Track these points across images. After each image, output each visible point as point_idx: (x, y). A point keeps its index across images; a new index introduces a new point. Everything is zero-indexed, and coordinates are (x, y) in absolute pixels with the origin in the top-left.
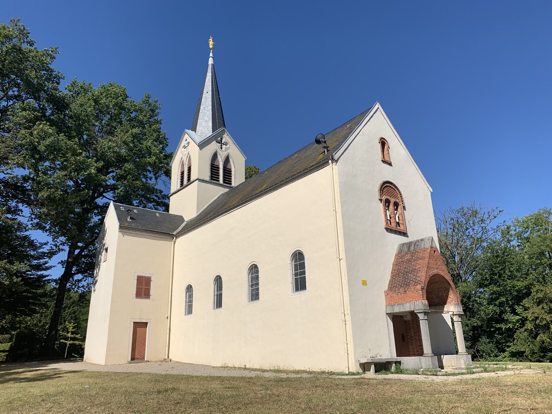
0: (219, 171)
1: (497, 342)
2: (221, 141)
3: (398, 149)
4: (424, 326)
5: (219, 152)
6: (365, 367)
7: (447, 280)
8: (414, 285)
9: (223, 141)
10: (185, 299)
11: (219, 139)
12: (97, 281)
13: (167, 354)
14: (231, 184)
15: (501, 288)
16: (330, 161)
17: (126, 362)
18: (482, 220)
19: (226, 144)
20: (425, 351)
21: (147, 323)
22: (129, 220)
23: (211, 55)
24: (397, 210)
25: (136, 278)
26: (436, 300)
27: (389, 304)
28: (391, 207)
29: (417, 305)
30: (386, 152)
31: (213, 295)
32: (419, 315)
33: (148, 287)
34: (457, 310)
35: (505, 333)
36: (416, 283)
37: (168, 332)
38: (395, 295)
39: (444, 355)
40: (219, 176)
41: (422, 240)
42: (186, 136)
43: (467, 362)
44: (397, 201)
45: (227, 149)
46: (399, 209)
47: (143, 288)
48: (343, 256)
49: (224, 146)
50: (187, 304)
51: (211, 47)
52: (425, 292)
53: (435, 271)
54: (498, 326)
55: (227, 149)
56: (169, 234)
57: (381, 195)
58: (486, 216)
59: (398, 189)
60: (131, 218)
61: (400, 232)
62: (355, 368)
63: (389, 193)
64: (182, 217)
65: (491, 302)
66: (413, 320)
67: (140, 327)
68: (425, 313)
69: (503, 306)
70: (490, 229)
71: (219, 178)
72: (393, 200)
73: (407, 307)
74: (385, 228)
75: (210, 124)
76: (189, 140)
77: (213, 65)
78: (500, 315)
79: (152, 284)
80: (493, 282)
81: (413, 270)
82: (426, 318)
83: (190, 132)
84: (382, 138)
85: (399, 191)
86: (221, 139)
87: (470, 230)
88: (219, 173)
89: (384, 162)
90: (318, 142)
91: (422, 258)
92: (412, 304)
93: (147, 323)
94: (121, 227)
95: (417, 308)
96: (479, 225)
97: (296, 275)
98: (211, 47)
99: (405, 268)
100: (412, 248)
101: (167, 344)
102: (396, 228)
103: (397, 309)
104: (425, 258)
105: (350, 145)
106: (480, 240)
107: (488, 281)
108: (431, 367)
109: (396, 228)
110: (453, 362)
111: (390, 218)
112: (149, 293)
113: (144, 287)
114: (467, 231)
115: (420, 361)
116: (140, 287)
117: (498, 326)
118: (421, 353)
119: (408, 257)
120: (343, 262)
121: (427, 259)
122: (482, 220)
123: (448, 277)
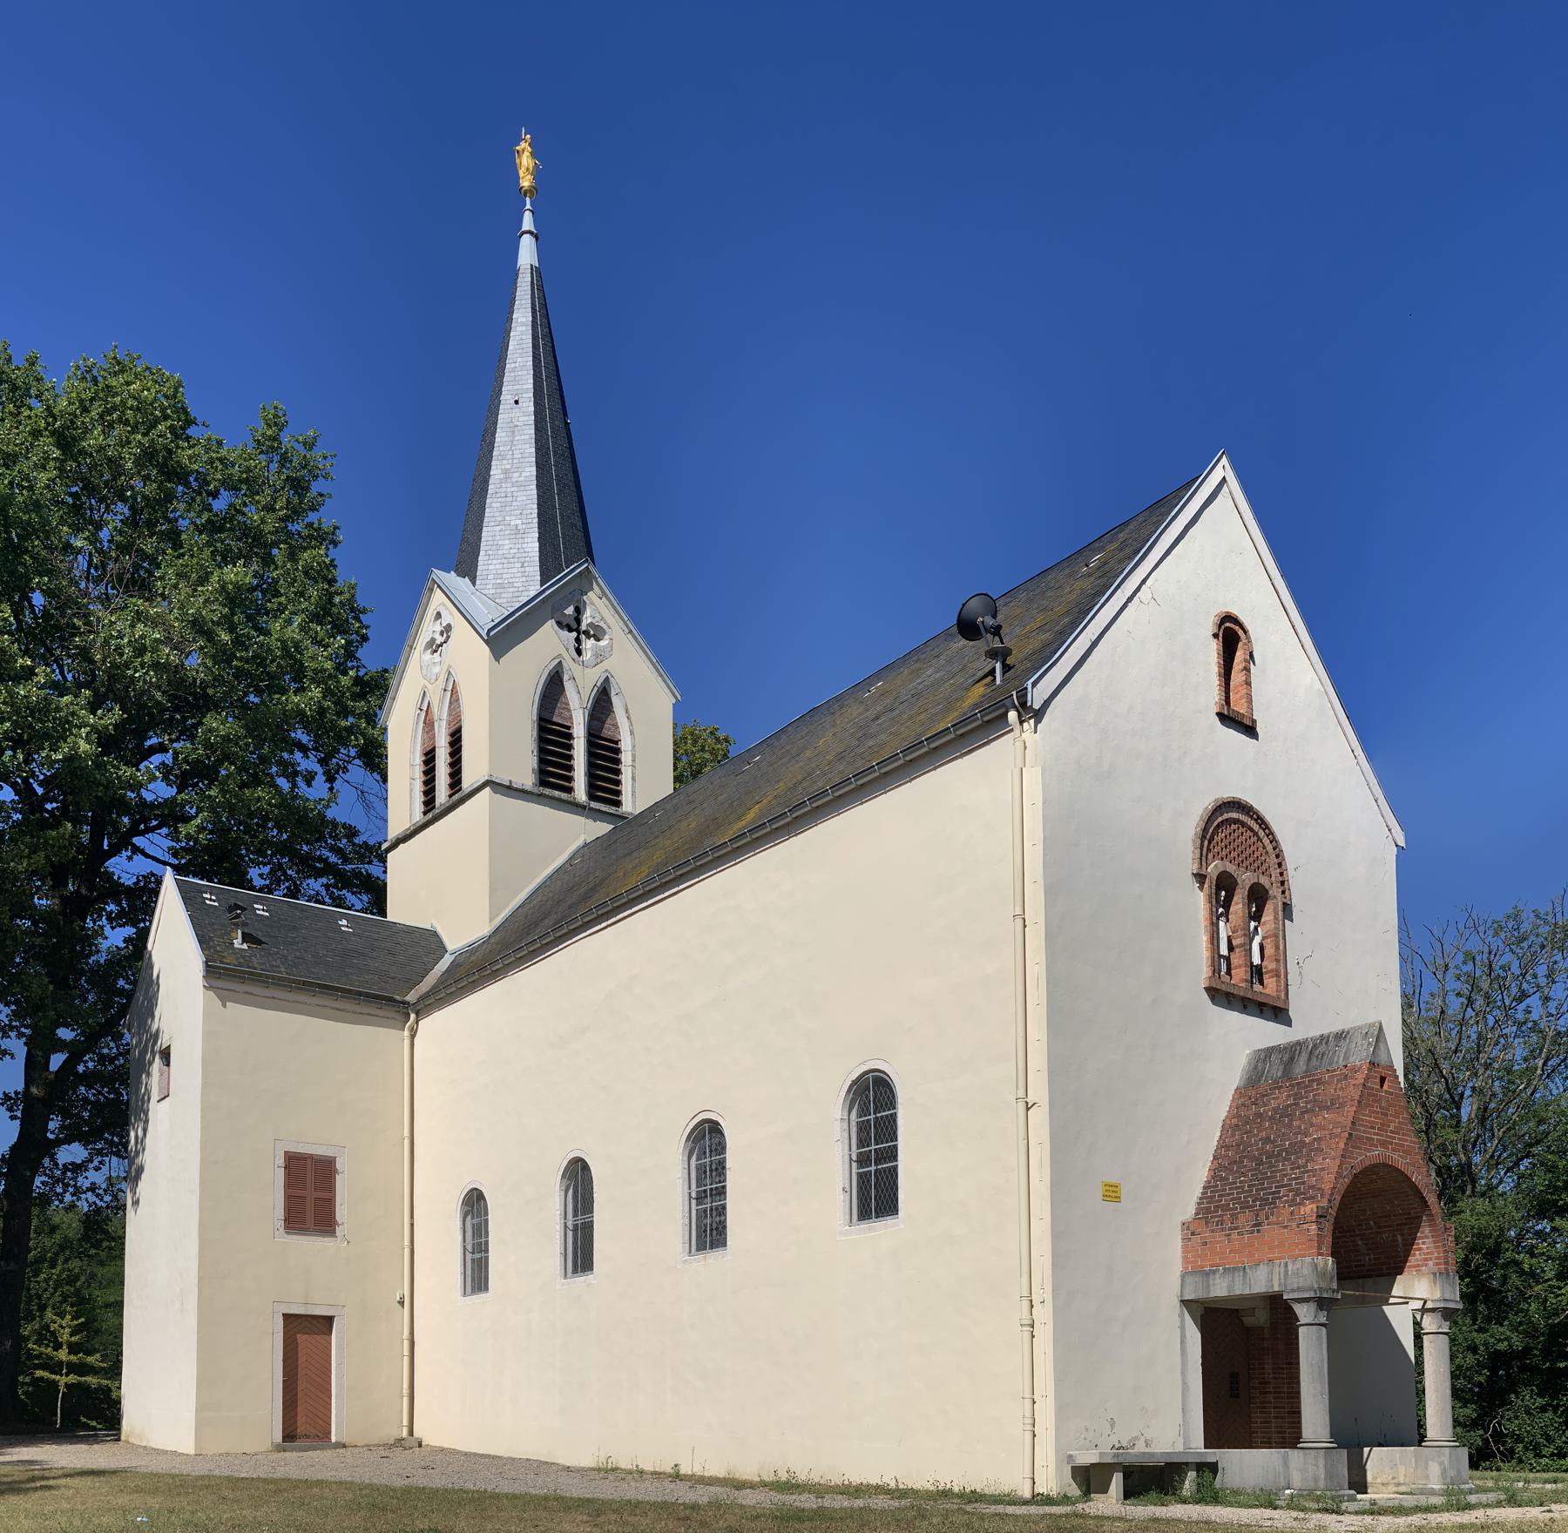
0: (570, 747)
2: (578, 621)
3: (1289, 667)
5: (571, 667)
6: (1090, 1478)
8: (1292, 1203)
9: (586, 620)
10: (459, 1237)
11: (570, 610)
14: (618, 804)
17: (267, 1445)
19: (597, 633)
22: (237, 943)
23: (528, 222)
24: (1257, 917)
25: (281, 1161)
27: (1195, 1270)
29: (1297, 1274)
30: (1237, 677)
31: (559, 1228)
33: (326, 1195)
34: (1438, 1295)
36: (1302, 1194)
41: (1340, 1036)
42: (438, 598)
43: (1452, 1473)
44: (1264, 881)
46: (1268, 916)
48: (1039, 1091)
49: (589, 644)
51: (526, 182)
52: (1328, 1226)
53: (1375, 1154)
55: (600, 657)
56: (391, 1000)
57: (1203, 859)
60: (246, 938)
62: (1052, 1479)
64: (435, 934)
68: (1322, 1303)
71: (570, 779)
72: (1246, 879)
73: (1260, 1281)
75: (532, 546)
76: (451, 616)
77: (537, 272)
82: (1323, 1320)
84: (1228, 618)
85: (1274, 840)
87: (1534, 1001)
88: (570, 758)
89: (1228, 718)
91: (1334, 1105)
92: (1278, 1270)
93: (329, 1320)
95: (1294, 1283)
97: (863, 1160)
98: (526, 182)
99: (1267, 1140)
100: (1300, 1067)
102: (1248, 990)
103: (1220, 1288)
104: (1342, 1105)
105: (1094, 644)
108: (1322, 1484)
109: (1248, 990)
110: (1402, 1469)
111: (1231, 948)
114: (1522, 1006)
115: (1286, 1463)
119: (1282, 1098)
120: (1040, 1119)
121: (1350, 1110)
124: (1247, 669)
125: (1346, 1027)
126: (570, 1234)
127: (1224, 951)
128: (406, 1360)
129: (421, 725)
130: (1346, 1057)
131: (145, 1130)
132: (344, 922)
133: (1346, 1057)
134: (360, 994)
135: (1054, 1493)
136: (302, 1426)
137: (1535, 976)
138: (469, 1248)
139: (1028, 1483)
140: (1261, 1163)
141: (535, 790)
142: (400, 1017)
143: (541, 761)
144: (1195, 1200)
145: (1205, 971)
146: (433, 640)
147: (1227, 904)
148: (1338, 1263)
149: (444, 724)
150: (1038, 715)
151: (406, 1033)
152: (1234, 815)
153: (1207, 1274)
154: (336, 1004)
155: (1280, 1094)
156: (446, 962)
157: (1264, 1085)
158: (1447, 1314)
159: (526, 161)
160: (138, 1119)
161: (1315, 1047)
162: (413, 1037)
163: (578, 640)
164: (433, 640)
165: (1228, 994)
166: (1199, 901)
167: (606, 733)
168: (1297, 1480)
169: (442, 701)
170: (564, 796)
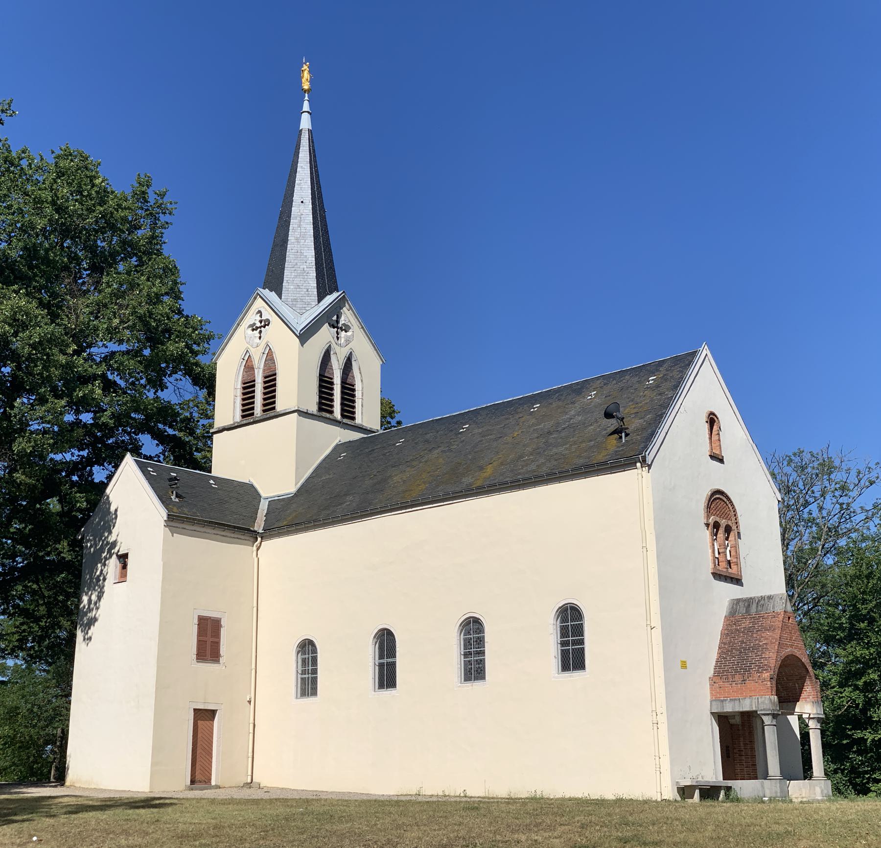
0: (332, 389)
1: (854, 770)
2: (338, 322)
3: (734, 432)
4: (771, 736)
5: (335, 348)
6: (685, 792)
7: (803, 664)
8: (758, 672)
9: (342, 321)
10: (295, 666)
11: (335, 318)
12: (95, 620)
13: (250, 773)
14: (353, 419)
15: (872, 650)
16: (638, 465)
17: (183, 787)
18: (843, 488)
19: (346, 328)
20: (771, 773)
21: (213, 713)
22: (173, 497)
23: (306, 106)
24: (727, 539)
25: (196, 621)
26: (788, 696)
27: (715, 699)
28: (721, 534)
29: (763, 703)
30: (715, 437)
31: (371, 664)
32: (764, 718)
33: (216, 640)
34: (815, 712)
35: (871, 750)
36: (761, 668)
37: (251, 731)
38: (727, 684)
39: (790, 780)
40: (332, 400)
41: (770, 597)
42: (259, 304)
43: (825, 792)
44: (730, 523)
45: (348, 341)
46: (731, 538)
47: (209, 640)
48: (656, 621)
49: (343, 334)
50: (299, 676)
51: (306, 86)
52: (774, 682)
53: (788, 651)
54: (858, 734)
55: (348, 341)
56: (249, 530)
57: (708, 517)
58: (853, 479)
59: (731, 502)
60: (177, 496)
61: (732, 578)
62: (670, 793)
63: (720, 510)
64: (252, 486)
65: (847, 679)
66: (743, 724)
67: (204, 717)
68: (775, 716)
69: (872, 691)
70: (859, 511)
71: (332, 406)
72: (723, 523)
73: (746, 705)
74: (712, 573)
75: (313, 284)
76: (268, 314)
78: (864, 711)
79: (223, 632)
80: (853, 635)
81: (756, 648)
83: (266, 292)
84: (712, 413)
85: (732, 505)
86: (338, 317)
87: (814, 507)
88: (332, 395)
89: (713, 457)
90: (608, 415)
91: (771, 629)
92: (754, 701)
93: (213, 713)
94: (171, 518)
95: (762, 707)
96: (834, 500)
97: (563, 644)
98: (306, 86)
99: (742, 642)
100: (753, 609)
101: (250, 755)
102: (728, 575)
103: (729, 708)
104: (774, 629)
106: (834, 532)
107: (844, 631)
108: (779, 795)
109: (728, 575)
110: (804, 790)
111: (719, 553)
112: (218, 650)
113: (209, 639)
114: (806, 510)
115: (763, 786)
116: (204, 639)
117: (858, 734)
118: (766, 776)
119: (747, 623)
120: (657, 635)
121: (778, 631)
122: (843, 488)
123: (805, 660)
124: (719, 434)
125: (772, 594)
126: (377, 668)
127: (717, 555)
128: (251, 735)
129: (243, 367)
130: (773, 608)
131: (99, 598)
132: (212, 482)
133: (773, 608)
134: (235, 527)
135: (671, 799)
136: (198, 777)
137: (813, 492)
138: (300, 672)
139: (659, 794)
140: (741, 652)
141: (319, 414)
142: (252, 539)
143: (320, 397)
144: (713, 667)
145: (711, 565)
146: (254, 324)
147: (716, 535)
148: (779, 698)
149: (261, 371)
150: (649, 466)
151: (255, 548)
152: (717, 496)
153: (722, 701)
154: (223, 533)
155: (744, 619)
156: (263, 507)
157: (738, 616)
158: (819, 720)
159: (306, 75)
160: (91, 588)
161: (759, 601)
162: (258, 549)
163: (338, 333)
164: (254, 324)
165: (720, 575)
166: (707, 534)
167: (349, 381)
168: (768, 793)
169: (260, 359)
170: (328, 415)
